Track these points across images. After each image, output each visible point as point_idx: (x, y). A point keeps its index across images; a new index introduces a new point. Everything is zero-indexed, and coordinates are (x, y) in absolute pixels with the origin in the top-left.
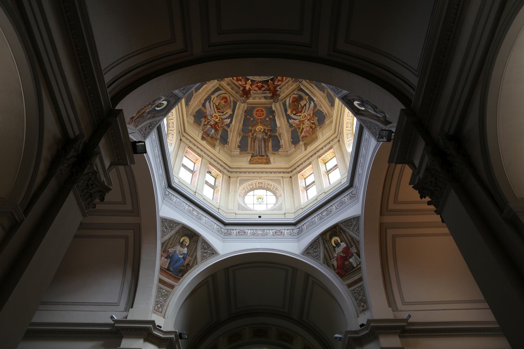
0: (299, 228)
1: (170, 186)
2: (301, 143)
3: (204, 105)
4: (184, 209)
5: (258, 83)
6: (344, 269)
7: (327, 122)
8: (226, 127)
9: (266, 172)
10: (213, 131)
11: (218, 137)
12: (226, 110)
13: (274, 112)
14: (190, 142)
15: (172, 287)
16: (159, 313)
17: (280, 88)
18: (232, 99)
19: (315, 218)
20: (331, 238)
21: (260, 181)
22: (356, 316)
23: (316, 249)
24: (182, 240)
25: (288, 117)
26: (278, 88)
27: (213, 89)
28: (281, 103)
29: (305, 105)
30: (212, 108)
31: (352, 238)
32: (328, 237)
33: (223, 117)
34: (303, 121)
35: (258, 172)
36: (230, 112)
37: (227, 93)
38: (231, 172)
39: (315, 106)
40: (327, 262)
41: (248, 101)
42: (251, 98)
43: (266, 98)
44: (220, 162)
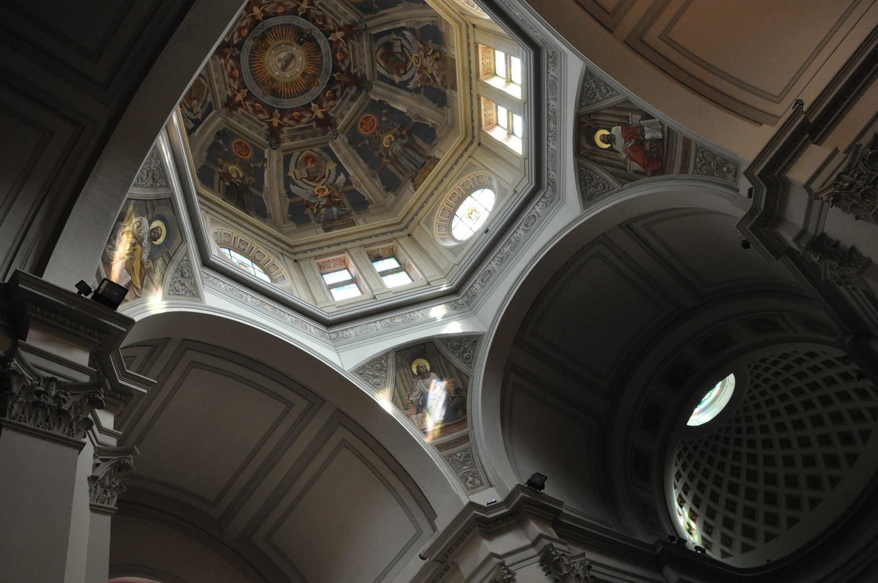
0: (548, 184)
1: (328, 324)
2: (448, 92)
3: (290, 194)
4: (377, 330)
5: (324, 96)
6: (656, 156)
7: (443, 28)
8: (348, 188)
9: (446, 176)
10: (335, 209)
11: (349, 208)
12: (325, 169)
13: (381, 102)
14: (312, 250)
15: (465, 438)
16: (478, 488)
17: (355, 67)
18: (317, 149)
19: (549, 145)
20: (593, 143)
21: (449, 194)
22: (735, 194)
23: (592, 181)
24: (415, 370)
25: (403, 85)
26: (353, 71)
27: (282, 165)
28: (376, 81)
29: (402, 46)
30: (305, 186)
31: (614, 107)
32: (589, 147)
33: (331, 180)
34: (421, 66)
35: (436, 189)
36: (332, 166)
37: (301, 150)
38: (406, 227)
39: (412, 30)
40: (625, 178)
41: (338, 128)
42: (338, 121)
43: (353, 99)
44: (377, 232)
